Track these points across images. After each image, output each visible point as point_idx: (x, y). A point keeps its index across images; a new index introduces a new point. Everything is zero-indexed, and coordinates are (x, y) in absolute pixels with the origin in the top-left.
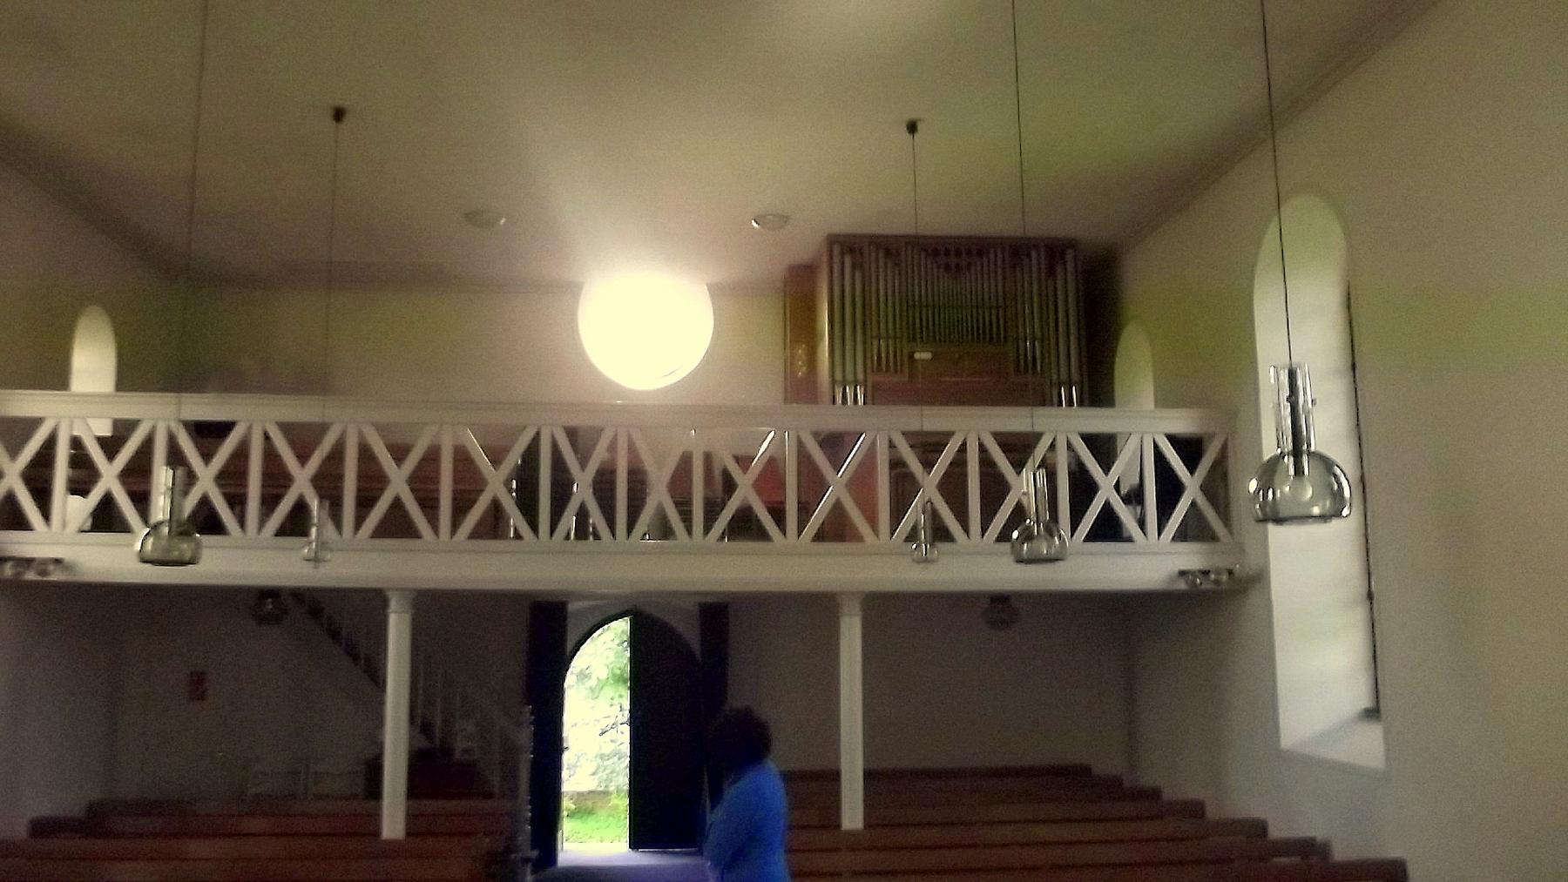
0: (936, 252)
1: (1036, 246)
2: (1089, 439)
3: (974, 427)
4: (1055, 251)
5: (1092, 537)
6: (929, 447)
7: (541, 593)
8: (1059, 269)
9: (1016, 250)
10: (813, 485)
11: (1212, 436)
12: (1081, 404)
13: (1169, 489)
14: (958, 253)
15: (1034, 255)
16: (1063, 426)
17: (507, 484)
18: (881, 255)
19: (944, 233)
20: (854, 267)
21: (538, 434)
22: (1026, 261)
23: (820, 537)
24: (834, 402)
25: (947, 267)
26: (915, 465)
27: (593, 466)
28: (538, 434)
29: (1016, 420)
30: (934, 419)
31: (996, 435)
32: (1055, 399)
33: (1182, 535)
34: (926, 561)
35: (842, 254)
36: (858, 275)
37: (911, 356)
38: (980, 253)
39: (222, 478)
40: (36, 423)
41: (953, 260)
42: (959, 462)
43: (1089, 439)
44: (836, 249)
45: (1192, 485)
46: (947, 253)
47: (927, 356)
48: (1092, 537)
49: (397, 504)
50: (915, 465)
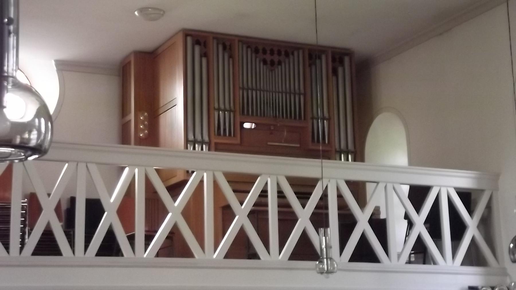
1: (298, 49)
2: (350, 184)
3: (272, 173)
4: (339, 56)
5: (354, 258)
6: (241, 184)
8: (340, 70)
9: (313, 53)
10: (156, 211)
11: (482, 191)
14: (272, 52)
15: (323, 57)
16: (333, 176)
18: (221, 48)
22: (318, 61)
25: (265, 62)
26: (232, 198)
27: (369, 211)
29: (305, 168)
33: (468, 261)
34: (328, 272)
35: (218, 44)
36: (204, 60)
41: (268, 57)
43: (350, 184)
44: (189, 39)
45: (472, 224)
48: (354, 258)
50: (232, 198)
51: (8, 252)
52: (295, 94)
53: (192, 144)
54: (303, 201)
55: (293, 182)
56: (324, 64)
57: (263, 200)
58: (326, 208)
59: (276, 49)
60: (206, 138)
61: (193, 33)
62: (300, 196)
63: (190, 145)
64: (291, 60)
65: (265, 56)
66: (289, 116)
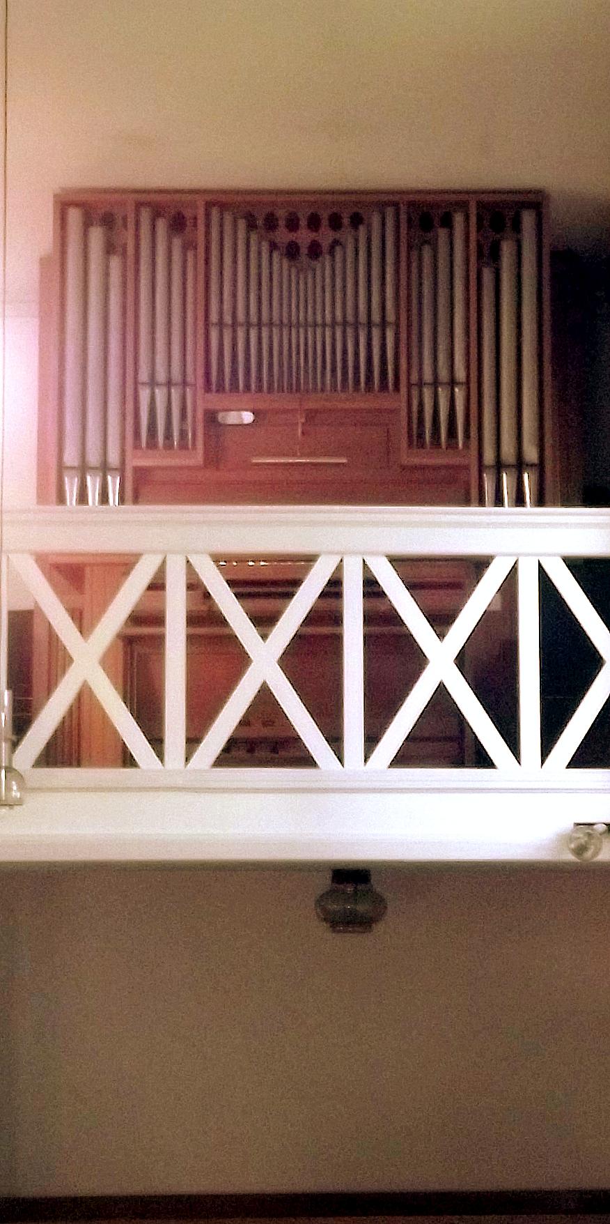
0: (271, 223)
1: (463, 206)
3: (358, 542)
6: (265, 587)
7: (340, 862)
8: (507, 249)
9: (424, 215)
12: (540, 501)
14: (314, 222)
15: (458, 219)
19: (421, 186)
20: (110, 249)
21: (514, 570)
22: (442, 233)
24: (61, 499)
25: (292, 252)
28: (514, 570)
31: (397, 561)
32: (474, 492)
35: (87, 225)
36: (115, 262)
38: (357, 220)
39: (292, 661)
40: (479, 565)
44: (74, 216)
51: (162, 760)
52: (345, 323)
53: (493, 471)
54: (441, 599)
56: (458, 241)
57: (330, 603)
58: (337, 619)
59: (281, 214)
60: (531, 454)
61: (223, 198)
62: (241, 590)
63: (72, 479)
65: (292, 236)
66: (351, 381)
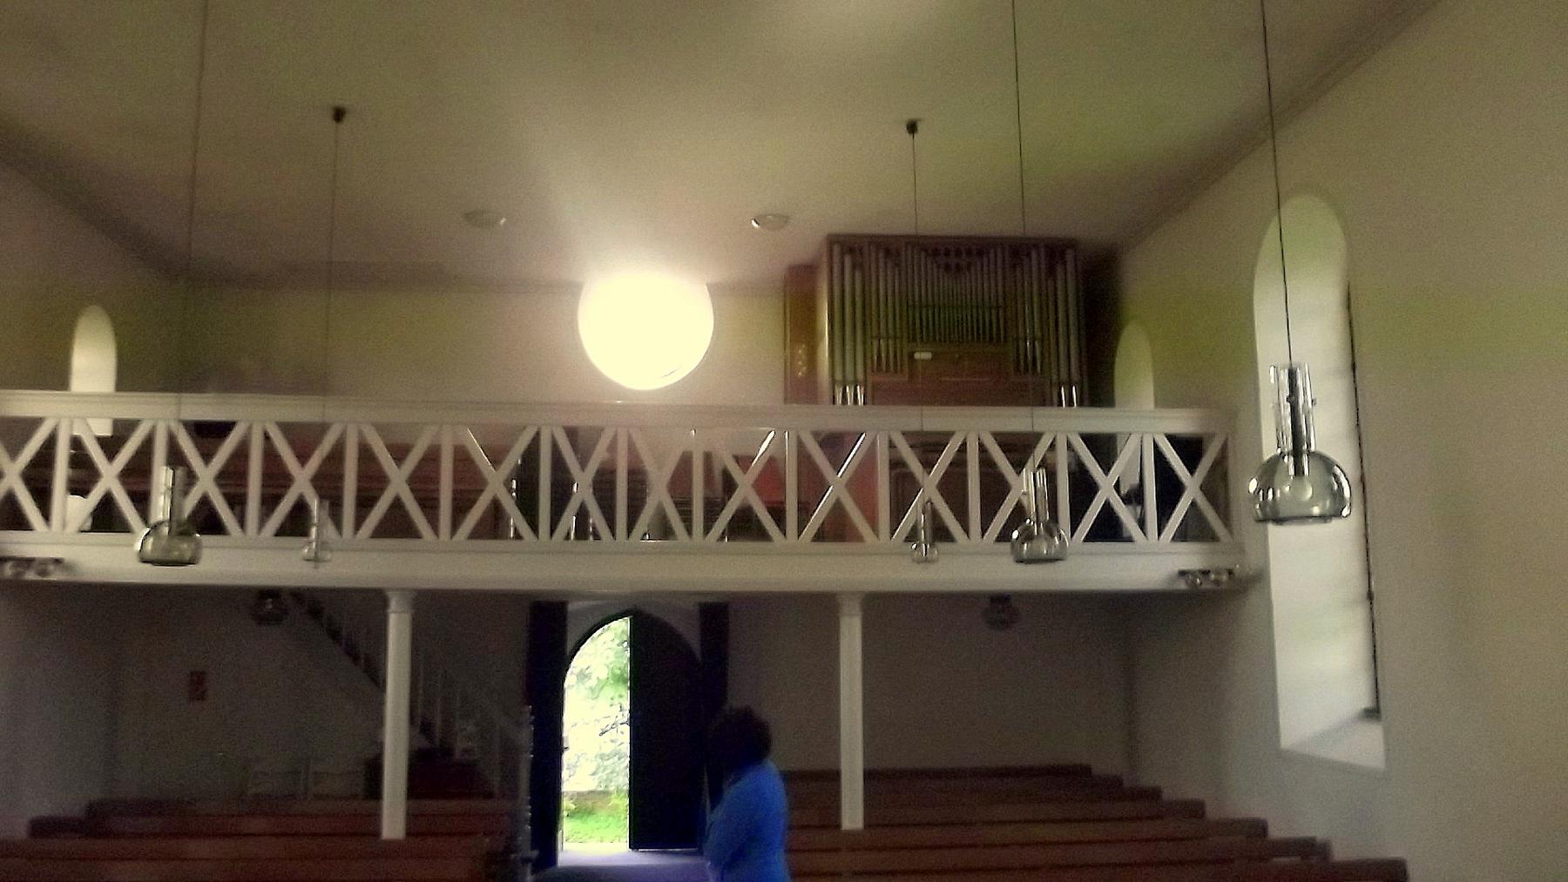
0: (936, 252)
1: (1036, 246)
2: (1089, 439)
3: (974, 427)
4: (1055, 251)
5: (1092, 537)
6: (929, 447)
7: (541, 593)
8: (1059, 269)
9: (1016, 250)
10: (813, 485)
11: (1212, 436)
12: (1081, 404)
13: (1169, 489)
14: (958, 253)
15: (1034, 255)
16: (1063, 426)
17: (507, 484)
18: (881, 255)
19: (944, 233)
20: (854, 267)
21: (538, 434)
22: (1026, 261)
23: (820, 537)
24: (834, 402)
25: (947, 267)
26: (915, 465)
27: (593, 466)
28: (538, 434)
29: (1016, 420)
30: (934, 419)
31: (996, 435)
32: (1055, 399)
33: (1182, 535)
35: (842, 254)
36: (858, 275)
37: (911, 356)
38: (980, 253)
39: (222, 478)
40: (36, 423)
41: (953, 260)
42: (959, 462)
43: (1089, 439)
44: (836, 249)
45: (1192, 485)
46: (947, 253)
47: (927, 356)
48: (1092, 537)
49: (397, 504)
50: (915, 465)
55: (287, 428)
64: (1034, 262)
